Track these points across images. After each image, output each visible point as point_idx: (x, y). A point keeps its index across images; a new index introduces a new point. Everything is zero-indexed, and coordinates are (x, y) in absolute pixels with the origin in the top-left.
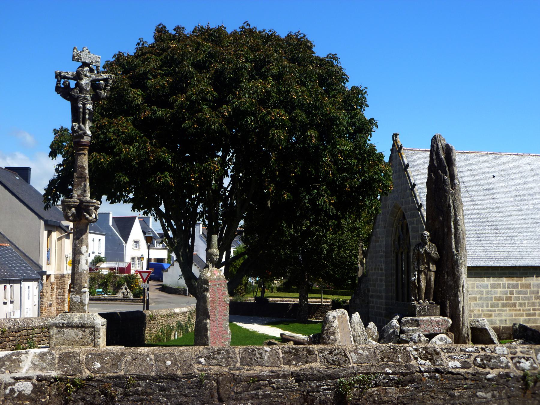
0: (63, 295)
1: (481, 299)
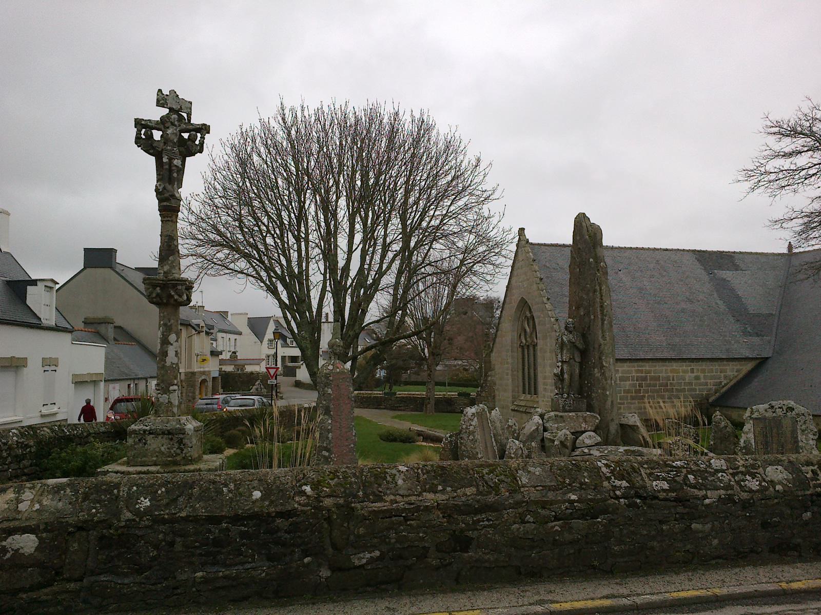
0: (194, 393)
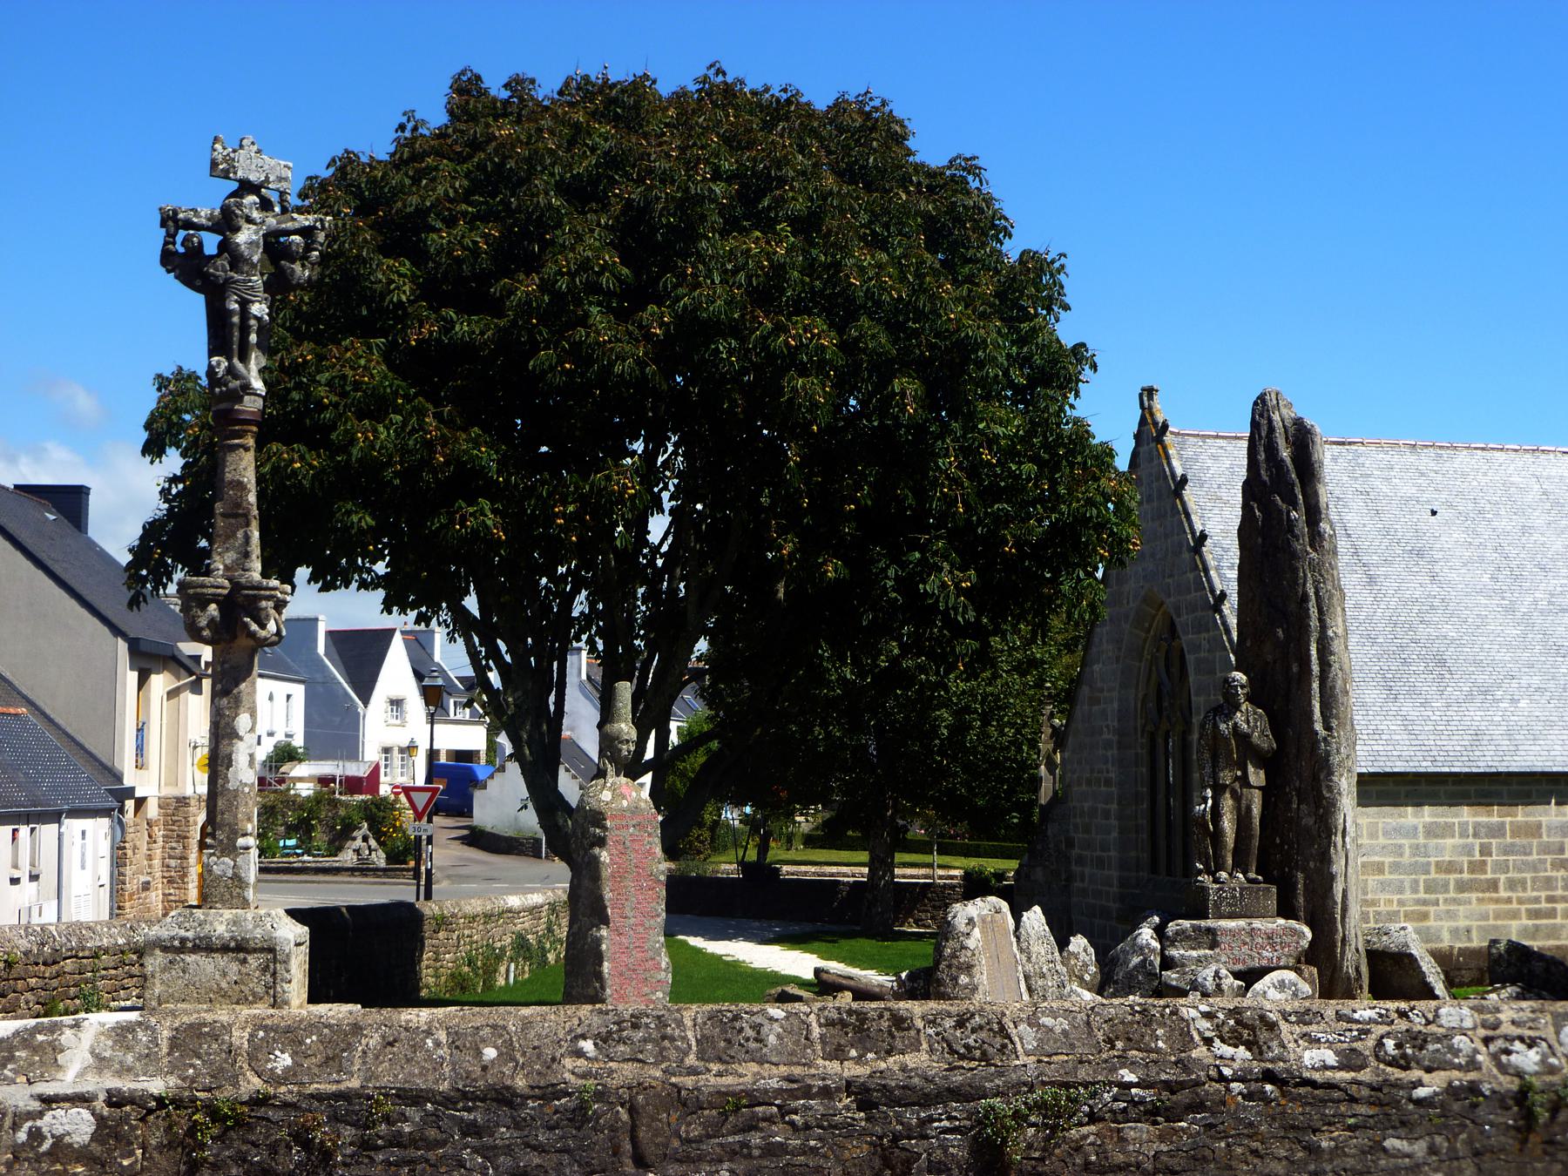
0: (184, 858)
1: (1396, 867)
